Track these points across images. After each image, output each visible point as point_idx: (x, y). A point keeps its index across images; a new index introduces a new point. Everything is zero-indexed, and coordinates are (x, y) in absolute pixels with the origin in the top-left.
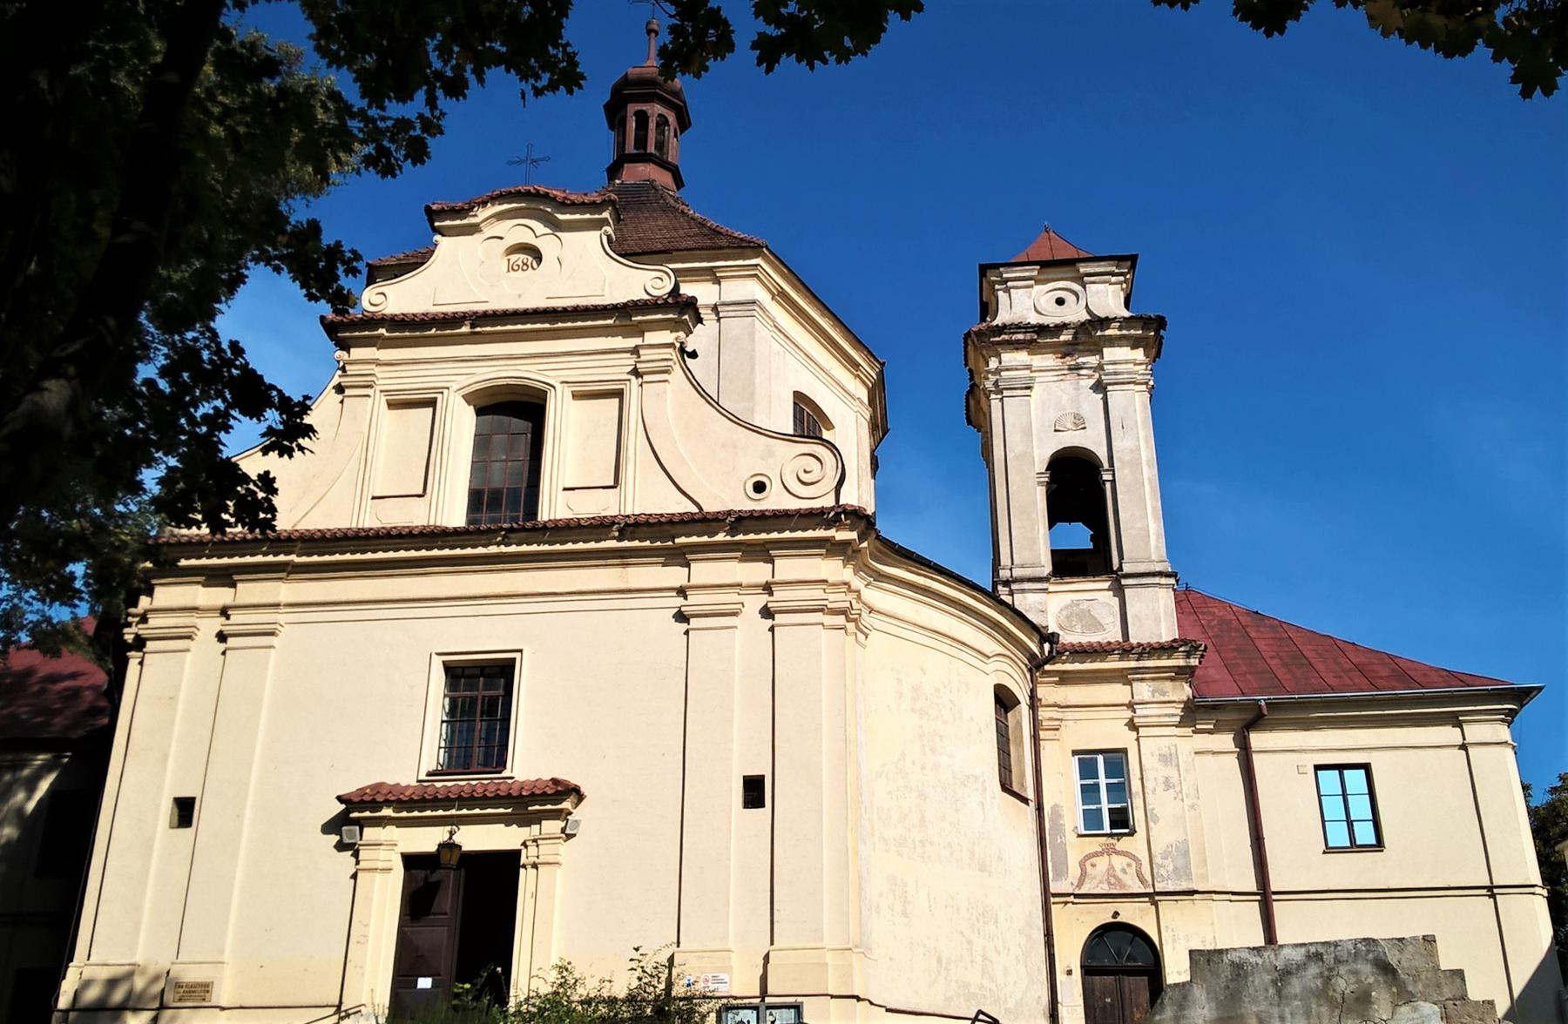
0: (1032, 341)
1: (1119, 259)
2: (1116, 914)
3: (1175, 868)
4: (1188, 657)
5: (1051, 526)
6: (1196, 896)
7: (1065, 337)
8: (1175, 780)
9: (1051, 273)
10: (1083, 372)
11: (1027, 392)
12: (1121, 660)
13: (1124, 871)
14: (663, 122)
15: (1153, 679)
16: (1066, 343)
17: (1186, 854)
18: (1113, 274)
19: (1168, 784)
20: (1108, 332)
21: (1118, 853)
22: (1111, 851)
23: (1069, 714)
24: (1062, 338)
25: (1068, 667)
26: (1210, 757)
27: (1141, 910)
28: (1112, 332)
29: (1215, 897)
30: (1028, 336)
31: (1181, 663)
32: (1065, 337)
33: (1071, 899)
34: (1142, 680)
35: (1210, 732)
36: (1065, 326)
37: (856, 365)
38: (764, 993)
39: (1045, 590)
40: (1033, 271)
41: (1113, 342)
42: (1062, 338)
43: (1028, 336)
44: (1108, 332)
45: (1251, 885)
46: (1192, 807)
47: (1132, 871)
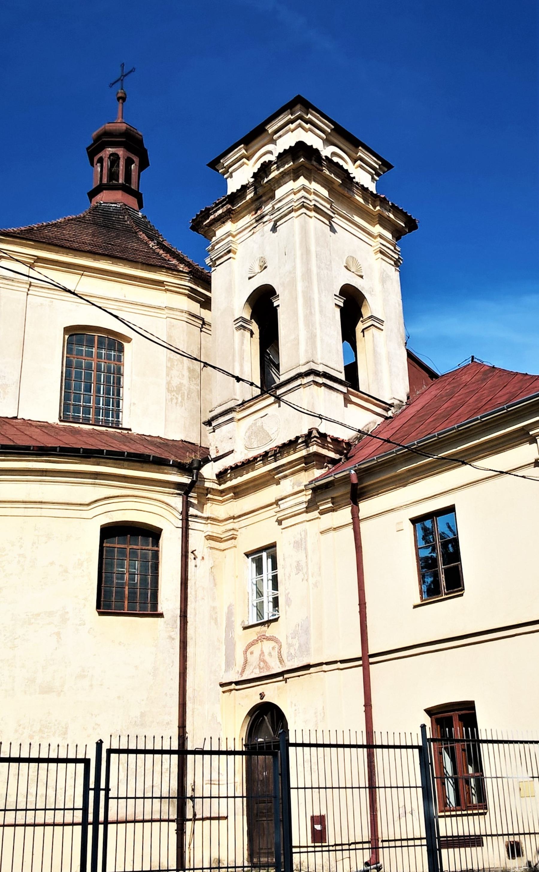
0: (229, 211)
1: (289, 107)
2: (262, 696)
3: (300, 646)
4: (308, 447)
5: (343, 341)
6: (312, 670)
7: (250, 196)
8: (303, 563)
9: (255, 145)
10: (265, 219)
11: (231, 255)
12: (265, 464)
13: (270, 654)
14: (129, 162)
15: (293, 473)
16: (253, 200)
17: (307, 631)
18: (292, 122)
19: (298, 567)
20: (271, 177)
21: (268, 639)
22: (263, 638)
23: (243, 522)
24: (248, 197)
25: (234, 482)
26: (332, 533)
27: (279, 688)
28: (274, 174)
29: (325, 667)
30: (225, 209)
31: (304, 453)
32: (250, 196)
33: (233, 686)
34: (285, 477)
35: (333, 510)
36: (244, 188)
37: (160, 283)
38: (182, 738)
39: (231, 420)
40: (241, 151)
41: (279, 182)
42: (248, 197)
43: (225, 209)
44: (271, 177)
45: (6, 823)
46: (316, 585)
47: (275, 653)
